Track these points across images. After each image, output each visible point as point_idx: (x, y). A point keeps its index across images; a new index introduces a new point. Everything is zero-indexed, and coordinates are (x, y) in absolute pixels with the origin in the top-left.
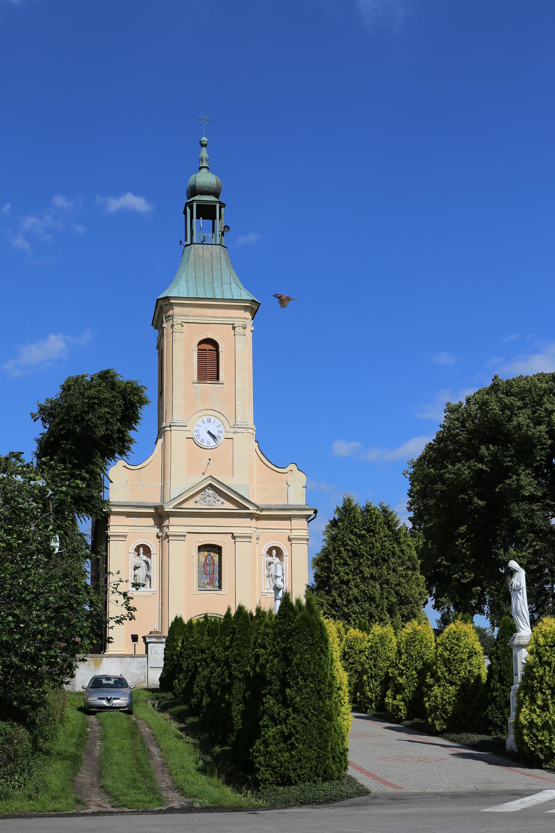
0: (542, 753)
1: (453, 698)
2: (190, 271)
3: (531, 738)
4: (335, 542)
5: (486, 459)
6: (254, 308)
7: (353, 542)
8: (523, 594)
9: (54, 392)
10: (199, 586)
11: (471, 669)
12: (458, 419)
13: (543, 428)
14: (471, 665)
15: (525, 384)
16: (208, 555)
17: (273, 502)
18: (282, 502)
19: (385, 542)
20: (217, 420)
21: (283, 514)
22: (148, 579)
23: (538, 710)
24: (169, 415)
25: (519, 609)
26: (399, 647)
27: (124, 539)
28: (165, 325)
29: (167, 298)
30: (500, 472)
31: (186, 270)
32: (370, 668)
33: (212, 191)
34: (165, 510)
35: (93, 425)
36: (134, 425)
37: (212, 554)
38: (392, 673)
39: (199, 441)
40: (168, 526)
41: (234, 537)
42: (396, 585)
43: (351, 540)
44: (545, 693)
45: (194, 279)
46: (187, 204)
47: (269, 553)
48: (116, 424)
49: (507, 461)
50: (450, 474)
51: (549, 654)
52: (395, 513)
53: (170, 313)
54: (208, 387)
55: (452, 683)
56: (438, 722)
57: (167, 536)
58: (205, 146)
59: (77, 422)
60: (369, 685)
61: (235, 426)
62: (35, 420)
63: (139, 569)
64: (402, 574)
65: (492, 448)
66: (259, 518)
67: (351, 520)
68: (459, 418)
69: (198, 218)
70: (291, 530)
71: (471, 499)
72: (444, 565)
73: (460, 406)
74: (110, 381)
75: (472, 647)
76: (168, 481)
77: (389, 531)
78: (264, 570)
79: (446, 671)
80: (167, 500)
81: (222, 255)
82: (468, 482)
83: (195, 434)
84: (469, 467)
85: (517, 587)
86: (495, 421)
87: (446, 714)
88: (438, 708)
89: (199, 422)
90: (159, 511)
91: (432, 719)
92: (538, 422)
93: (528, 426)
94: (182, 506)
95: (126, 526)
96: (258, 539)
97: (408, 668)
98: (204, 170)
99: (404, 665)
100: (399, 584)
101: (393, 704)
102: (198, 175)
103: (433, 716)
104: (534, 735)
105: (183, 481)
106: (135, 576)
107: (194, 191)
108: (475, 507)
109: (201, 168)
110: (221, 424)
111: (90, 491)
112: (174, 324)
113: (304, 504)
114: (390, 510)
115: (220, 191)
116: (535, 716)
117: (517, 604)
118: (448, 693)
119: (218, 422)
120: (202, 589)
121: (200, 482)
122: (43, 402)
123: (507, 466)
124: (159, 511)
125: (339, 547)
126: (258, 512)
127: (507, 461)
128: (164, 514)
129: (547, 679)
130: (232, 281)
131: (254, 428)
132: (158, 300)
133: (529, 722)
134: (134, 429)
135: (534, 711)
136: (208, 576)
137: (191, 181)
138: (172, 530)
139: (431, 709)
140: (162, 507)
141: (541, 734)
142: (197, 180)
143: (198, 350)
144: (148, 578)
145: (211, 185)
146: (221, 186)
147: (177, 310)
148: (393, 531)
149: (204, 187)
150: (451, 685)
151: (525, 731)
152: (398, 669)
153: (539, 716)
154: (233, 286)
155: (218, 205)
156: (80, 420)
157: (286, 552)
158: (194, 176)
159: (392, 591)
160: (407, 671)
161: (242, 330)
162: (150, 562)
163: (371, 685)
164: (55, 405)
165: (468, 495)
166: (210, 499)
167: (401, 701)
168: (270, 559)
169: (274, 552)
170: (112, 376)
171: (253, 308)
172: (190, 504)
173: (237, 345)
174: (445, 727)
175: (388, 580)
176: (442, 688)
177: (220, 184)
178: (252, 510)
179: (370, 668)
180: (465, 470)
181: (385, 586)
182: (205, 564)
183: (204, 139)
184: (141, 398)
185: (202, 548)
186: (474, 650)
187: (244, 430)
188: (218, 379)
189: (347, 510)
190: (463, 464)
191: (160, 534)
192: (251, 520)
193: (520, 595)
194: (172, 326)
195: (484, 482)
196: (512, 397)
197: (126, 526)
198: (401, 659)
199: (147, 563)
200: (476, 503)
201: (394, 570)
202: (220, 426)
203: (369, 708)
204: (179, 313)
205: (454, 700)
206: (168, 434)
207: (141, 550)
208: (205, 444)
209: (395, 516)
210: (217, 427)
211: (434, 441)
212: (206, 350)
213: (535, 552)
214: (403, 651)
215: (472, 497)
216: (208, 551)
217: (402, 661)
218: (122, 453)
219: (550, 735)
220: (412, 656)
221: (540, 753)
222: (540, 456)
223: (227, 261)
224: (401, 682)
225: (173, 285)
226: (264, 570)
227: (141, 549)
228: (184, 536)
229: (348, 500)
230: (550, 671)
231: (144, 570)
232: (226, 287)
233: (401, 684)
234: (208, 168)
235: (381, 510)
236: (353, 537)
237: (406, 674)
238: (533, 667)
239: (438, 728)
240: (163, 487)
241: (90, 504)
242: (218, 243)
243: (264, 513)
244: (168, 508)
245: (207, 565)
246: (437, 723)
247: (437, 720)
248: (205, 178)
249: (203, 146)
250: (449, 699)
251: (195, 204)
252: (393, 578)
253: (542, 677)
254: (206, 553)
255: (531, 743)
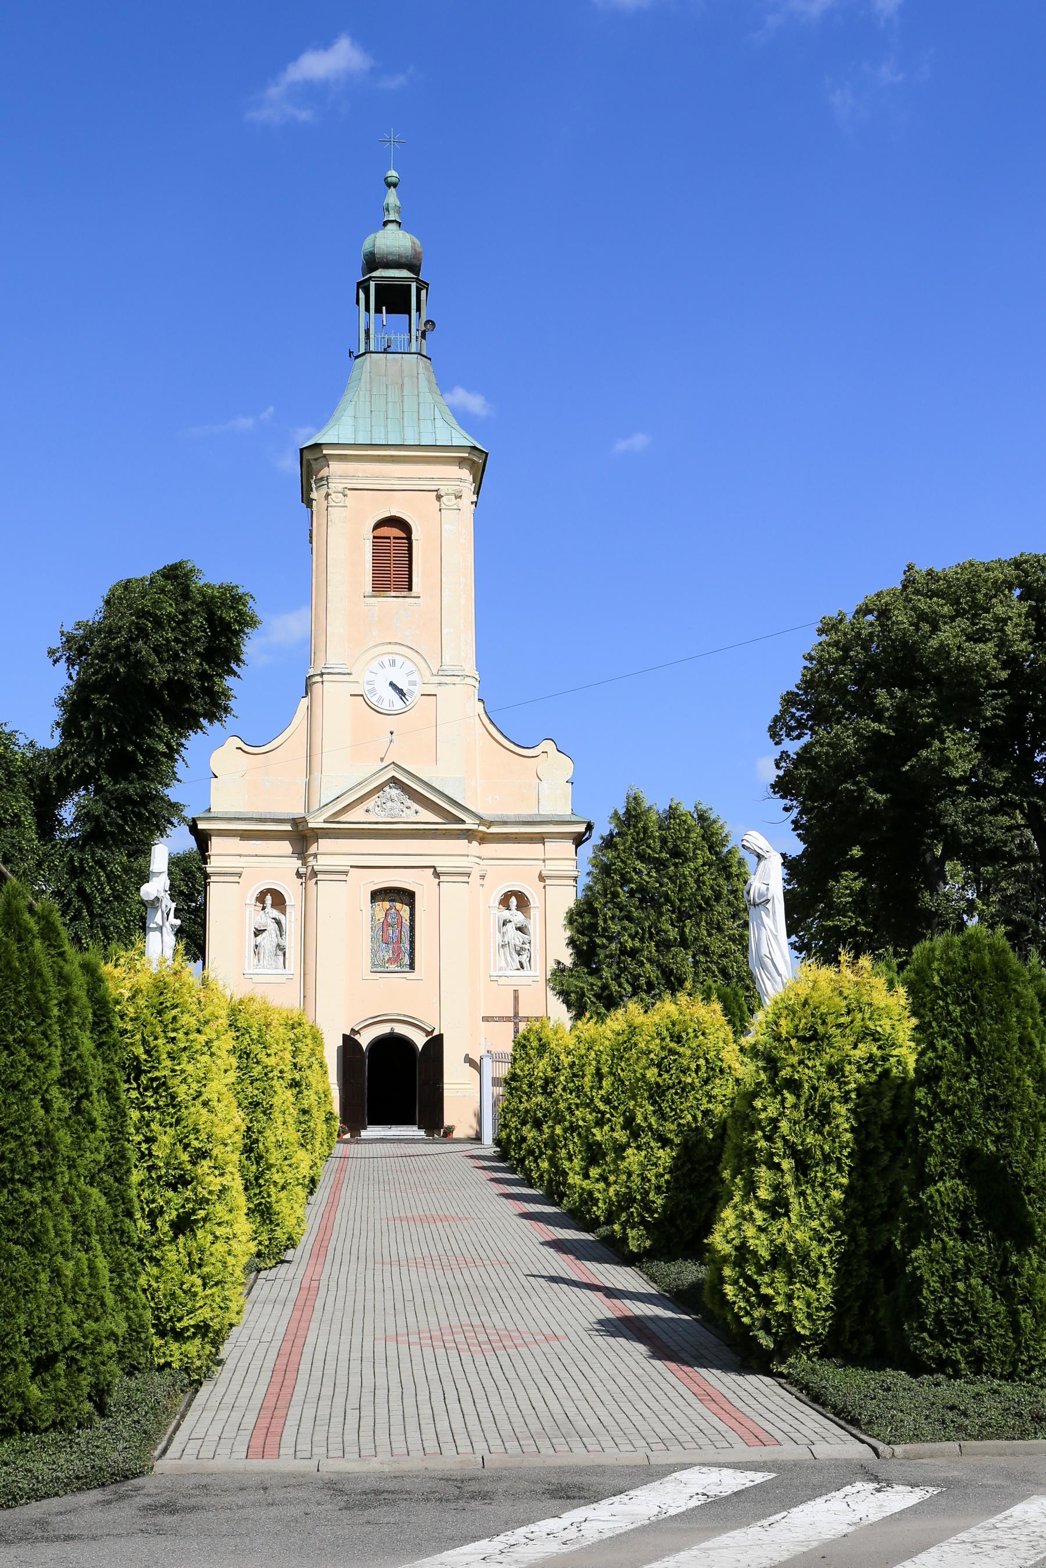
0: (768, 1332)
1: (667, 1177)
2: (362, 399)
3: (742, 1290)
4: (608, 875)
5: (887, 714)
6: (477, 462)
7: (645, 874)
8: (774, 913)
9: (89, 609)
10: (374, 965)
11: (711, 1106)
12: (836, 644)
13: (990, 647)
14: (711, 1098)
15: (957, 573)
16: (391, 908)
17: (511, 811)
18: (528, 810)
19: (703, 875)
20: (407, 661)
21: (530, 833)
22: (281, 953)
23: (759, 1215)
24: (321, 655)
25: (764, 950)
26: (599, 1062)
27: (236, 879)
28: (314, 495)
29: (317, 446)
30: (910, 736)
31: (355, 399)
32: (569, 1108)
33: (404, 260)
34: (310, 825)
35: (159, 670)
36: (233, 666)
37: (398, 905)
38: (584, 1120)
39: (374, 700)
40: (315, 855)
41: (437, 875)
42: (721, 956)
43: (639, 873)
44: (777, 1167)
45: (368, 412)
46: (359, 284)
47: (505, 902)
48: (194, 662)
49: (924, 716)
50: (822, 746)
51: (794, 1059)
52: (721, 822)
53: (324, 473)
54: (391, 604)
55: (665, 1142)
56: (634, 1232)
57: (315, 874)
58: (395, 185)
59: (120, 658)
60: (565, 1145)
61: (440, 673)
62: (55, 662)
63: (264, 934)
64: (734, 935)
65: (899, 694)
66: (484, 839)
67: (638, 834)
68: (839, 642)
69: (378, 311)
70: (544, 861)
71: (862, 791)
72: (862, 932)
73: (841, 621)
74: (182, 584)
75: (717, 1056)
76: (316, 774)
77: (711, 853)
78: (495, 934)
79: (654, 1112)
80: (315, 806)
81: (421, 370)
82: (856, 760)
83: (368, 687)
84: (856, 732)
85: (760, 895)
86: (904, 643)
87: (651, 1211)
88: (634, 1200)
89: (375, 666)
90: (300, 828)
91: (621, 1224)
92: (977, 637)
93: (959, 648)
94: (342, 819)
95: (240, 856)
96: (483, 877)
97: (615, 1108)
98: (391, 227)
99: (607, 1101)
100: (724, 955)
101: (583, 1189)
102: (380, 234)
103: (624, 1217)
104: (750, 1281)
105: (344, 770)
106: (256, 946)
107: (372, 262)
108: (872, 805)
109: (385, 224)
110: (414, 668)
111: (144, 786)
112: (330, 491)
113: (570, 813)
114: (713, 817)
115: (420, 260)
116: (750, 1231)
117: (759, 938)
118: (655, 1164)
119: (409, 666)
120: (379, 969)
121: (375, 774)
122: (69, 628)
123: (925, 723)
124: (300, 828)
125: (614, 885)
126: (482, 828)
127: (924, 716)
128: (309, 834)
129: (784, 1126)
130: (438, 415)
131: (477, 677)
132: (302, 450)
133: (737, 1248)
134: (235, 674)
135: (749, 1217)
136: (391, 946)
137: (367, 246)
138: (322, 863)
139: (619, 1202)
140: (304, 820)
141: (766, 1279)
142: (377, 243)
143: (374, 537)
144: (281, 950)
145: (402, 251)
146: (420, 253)
147: (335, 468)
148: (717, 854)
149: (390, 254)
150: (663, 1147)
151: (727, 1272)
152: (594, 1111)
153: (761, 1229)
154: (439, 423)
155: (414, 285)
156: (125, 654)
157: (535, 901)
158: (372, 236)
159: (714, 968)
160: (612, 1115)
161: (454, 501)
162: (283, 922)
163: (571, 1147)
164: (92, 632)
165: (855, 783)
166: (393, 804)
167: (597, 1180)
168: (506, 914)
169: (513, 901)
170: (186, 575)
171: (474, 462)
172: (357, 815)
173: (444, 527)
174: (648, 1243)
175: (706, 947)
176: (643, 1153)
177: (418, 249)
178: (470, 824)
179: (569, 1108)
180: (848, 737)
181: (702, 958)
182: (385, 925)
183: (393, 174)
184: (241, 613)
185: (377, 895)
186: (720, 1063)
187: (457, 680)
188: (410, 589)
189: (632, 817)
190: (845, 726)
191: (302, 870)
192: (470, 842)
193: (768, 916)
194: (328, 495)
195: (883, 756)
196: (935, 599)
197: (240, 856)
198: (601, 1088)
199: (278, 923)
200: (872, 798)
201: (720, 929)
202: (412, 672)
203: (566, 1195)
204: (339, 473)
205: (667, 1182)
206: (317, 689)
207: (269, 899)
208: (384, 706)
209: (722, 827)
210: (408, 674)
211: (797, 687)
212: (389, 538)
213: (1005, 901)
214: (605, 1070)
215: (865, 789)
216: (390, 901)
217: (603, 1092)
218: (212, 717)
219: (790, 1282)
220: (623, 1082)
221: (761, 1334)
222: (994, 709)
223: (429, 381)
224: (599, 1138)
225: (331, 423)
226: (495, 934)
227: (269, 898)
228: (346, 873)
229: (635, 798)
230: (795, 1106)
231: (274, 935)
232: (426, 426)
233: (599, 1144)
234: (399, 224)
235: (695, 816)
236: (639, 865)
237: (609, 1120)
238: (754, 1095)
239: (633, 1246)
240: (308, 785)
241: (147, 810)
242: (413, 350)
243: (493, 830)
244: (316, 822)
245: (389, 925)
246: (632, 1233)
247: (632, 1228)
248: (392, 240)
249: (389, 185)
250: (656, 1177)
251: (372, 284)
252: (716, 944)
253: (774, 1121)
254: (387, 905)
255: (742, 1305)
